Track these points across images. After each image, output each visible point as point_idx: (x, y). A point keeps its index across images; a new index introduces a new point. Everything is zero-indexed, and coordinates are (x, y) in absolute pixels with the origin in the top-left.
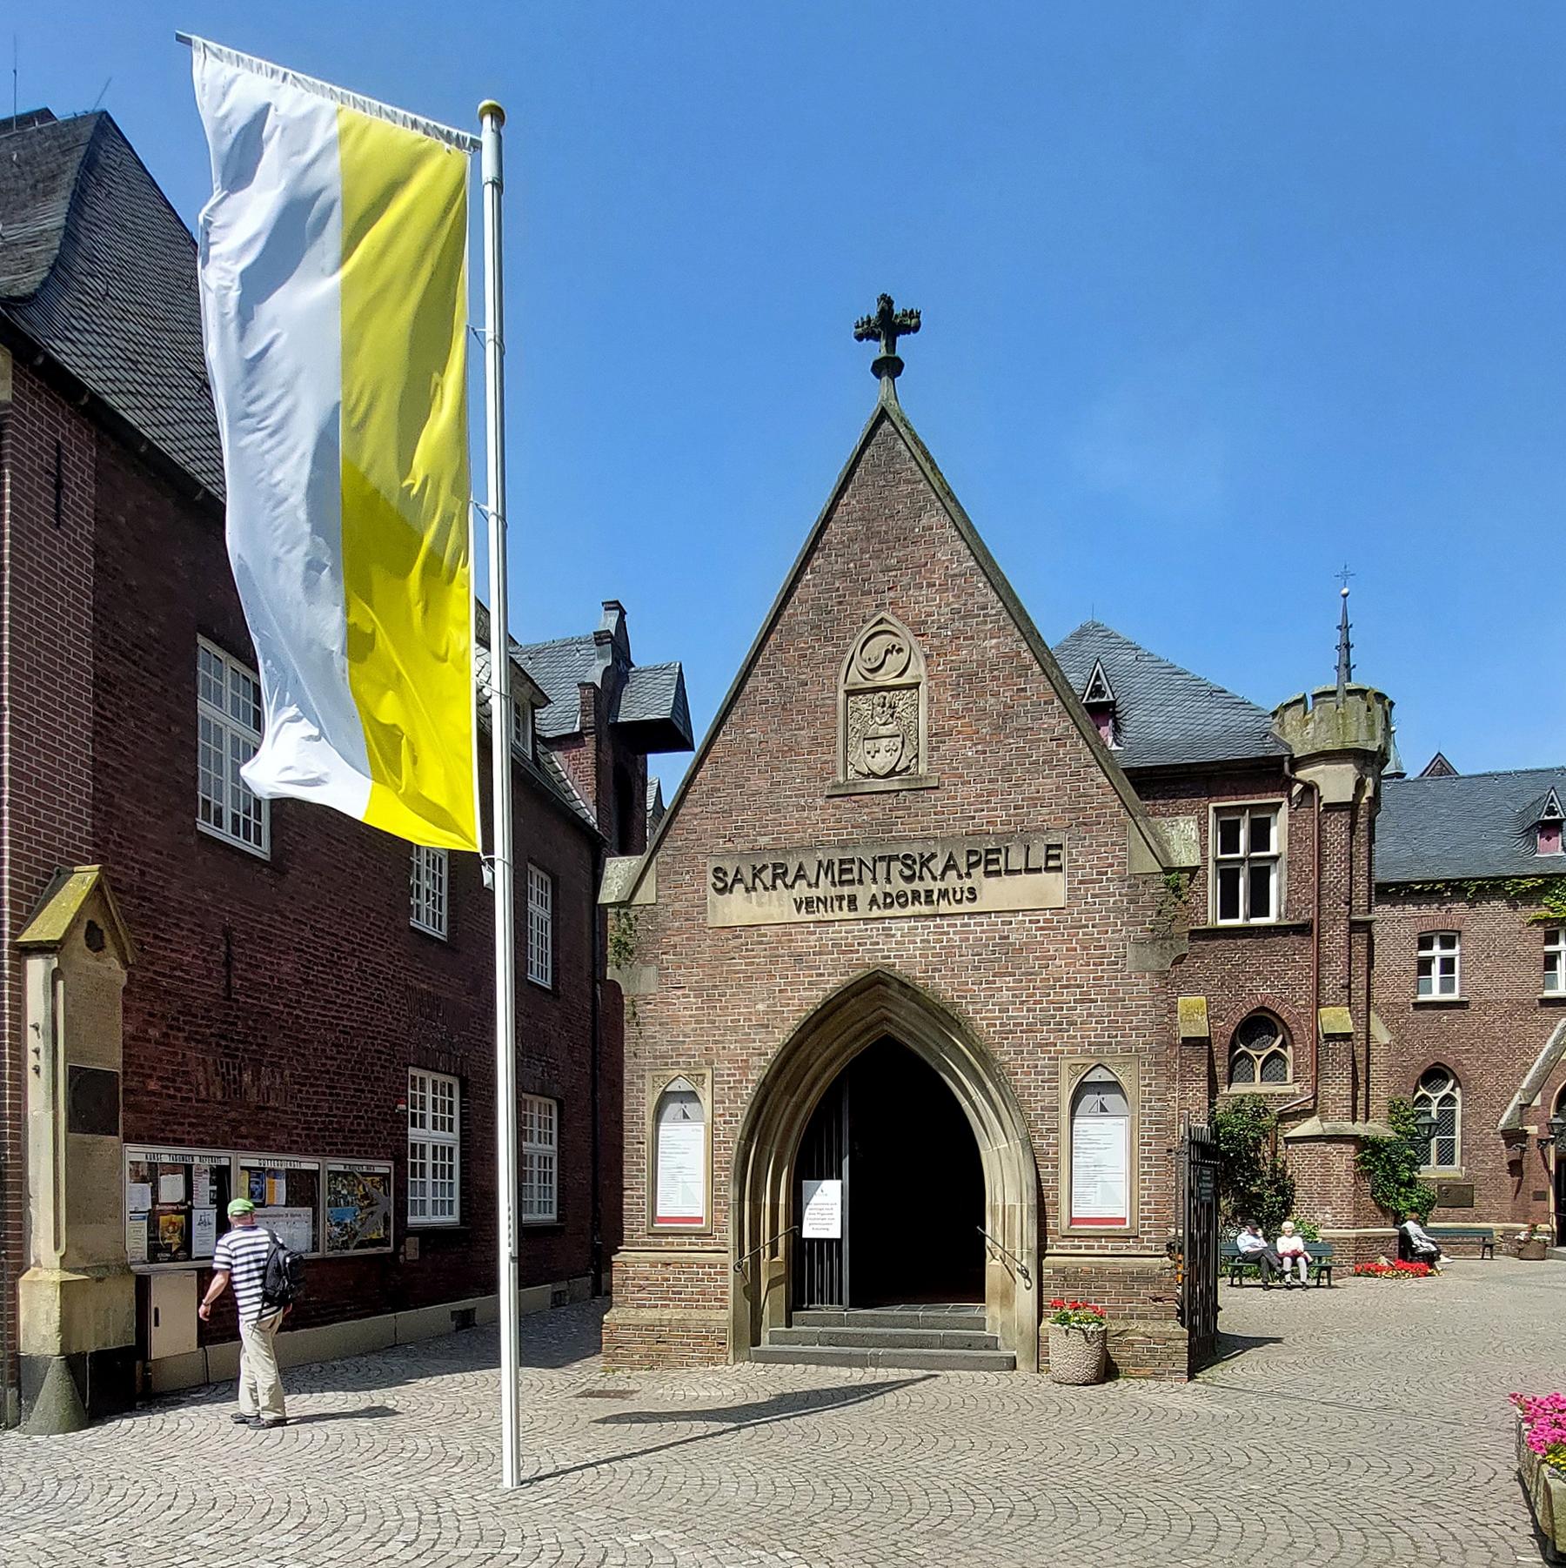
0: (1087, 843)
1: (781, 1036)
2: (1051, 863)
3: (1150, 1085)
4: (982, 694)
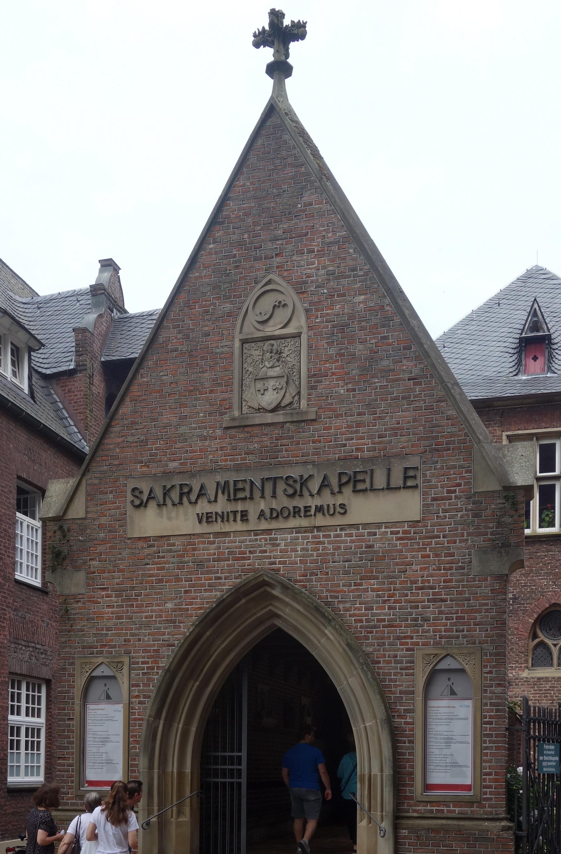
0: (439, 465)
1: (186, 628)
2: (409, 483)
3: (490, 672)
4: (352, 342)
